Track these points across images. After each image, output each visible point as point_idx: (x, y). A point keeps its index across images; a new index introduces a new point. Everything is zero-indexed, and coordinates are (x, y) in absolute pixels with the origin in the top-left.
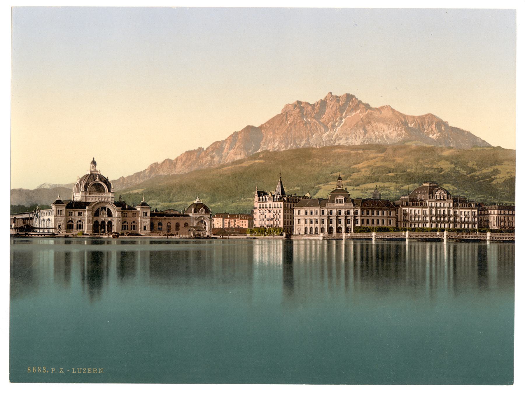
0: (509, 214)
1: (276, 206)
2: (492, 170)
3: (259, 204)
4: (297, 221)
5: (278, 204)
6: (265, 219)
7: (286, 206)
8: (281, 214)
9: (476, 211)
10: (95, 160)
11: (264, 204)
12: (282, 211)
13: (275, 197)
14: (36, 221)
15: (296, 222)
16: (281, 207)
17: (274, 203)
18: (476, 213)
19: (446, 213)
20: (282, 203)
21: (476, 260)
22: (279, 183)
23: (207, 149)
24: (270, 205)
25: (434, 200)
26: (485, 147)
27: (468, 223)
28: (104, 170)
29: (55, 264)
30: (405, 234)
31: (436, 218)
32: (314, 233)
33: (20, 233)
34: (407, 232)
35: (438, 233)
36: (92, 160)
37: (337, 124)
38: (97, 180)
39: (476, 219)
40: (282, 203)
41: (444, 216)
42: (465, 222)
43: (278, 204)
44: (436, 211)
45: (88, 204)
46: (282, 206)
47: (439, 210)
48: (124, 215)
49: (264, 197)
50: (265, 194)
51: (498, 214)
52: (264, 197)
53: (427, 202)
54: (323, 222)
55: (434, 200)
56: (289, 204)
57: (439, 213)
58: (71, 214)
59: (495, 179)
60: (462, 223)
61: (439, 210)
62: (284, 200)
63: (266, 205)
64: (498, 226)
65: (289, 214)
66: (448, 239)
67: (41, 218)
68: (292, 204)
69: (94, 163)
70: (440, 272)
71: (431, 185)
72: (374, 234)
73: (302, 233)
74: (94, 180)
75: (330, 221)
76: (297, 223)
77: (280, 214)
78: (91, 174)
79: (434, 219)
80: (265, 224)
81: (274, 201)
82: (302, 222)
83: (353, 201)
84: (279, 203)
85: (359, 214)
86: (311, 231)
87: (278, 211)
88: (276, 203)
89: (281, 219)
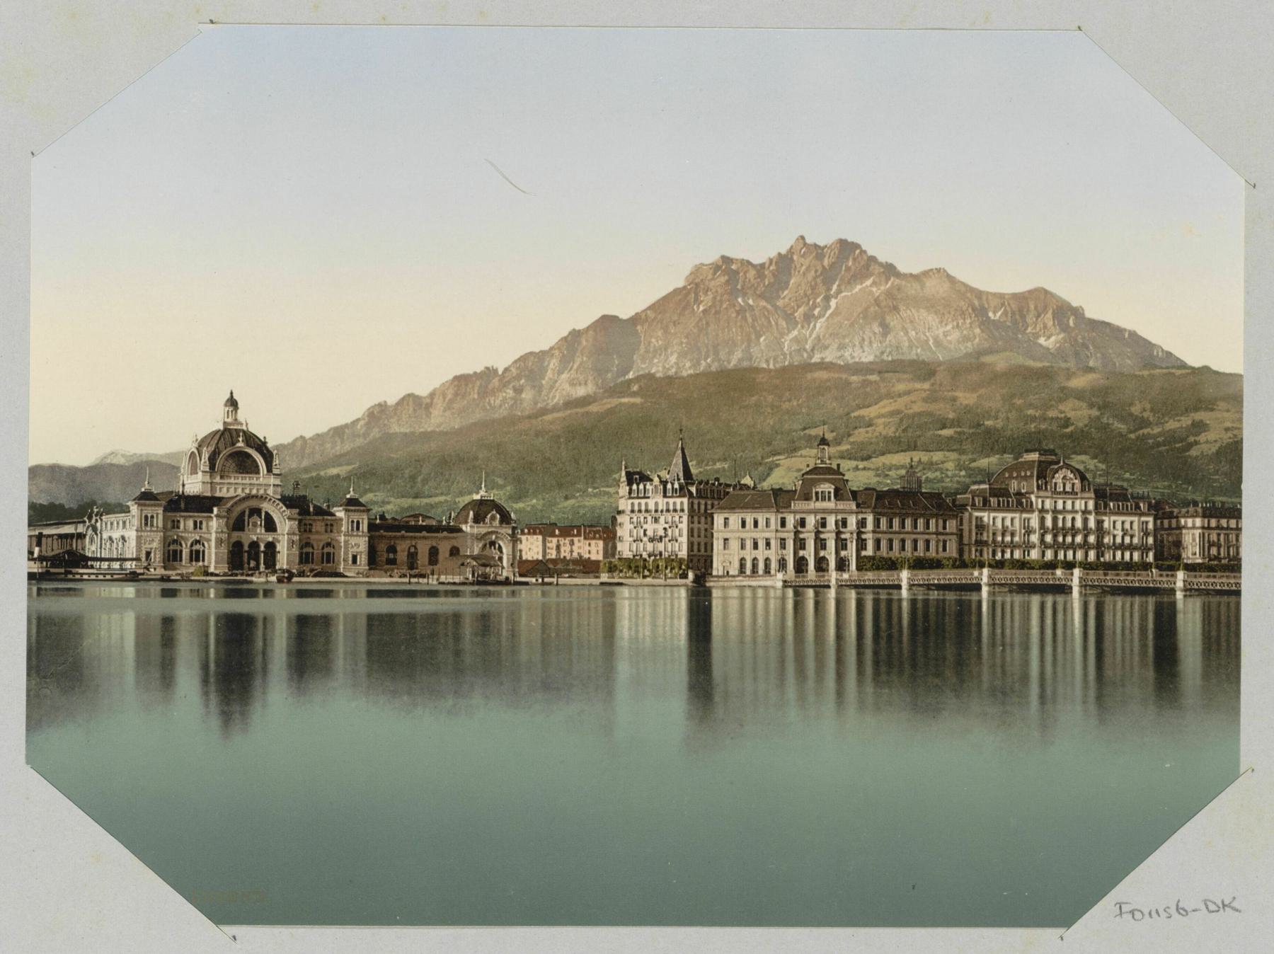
1: (671, 508)
2: (1190, 422)
4: (721, 542)
5: (675, 504)
7: (696, 507)
8: (684, 526)
10: (235, 397)
11: (643, 501)
12: (685, 519)
13: (669, 486)
14: (92, 541)
15: (718, 545)
16: (682, 510)
18: (1151, 526)
19: (1079, 524)
20: (685, 500)
22: (679, 452)
23: (506, 370)
24: (656, 504)
26: (1173, 367)
30: (981, 574)
31: (1055, 536)
32: (761, 572)
33: (52, 570)
34: (1077, 572)
35: (1059, 572)
36: (228, 396)
37: (816, 312)
39: (1151, 540)
40: (685, 500)
42: (1123, 547)
43: (675, 504)
44: (1055, 520)
45: (218, 501)
46: (686, 507)
50: (645, 478)
51: (1203, 528)
52: (641, 486)
53: (1033, 499)
54: (783, 546)
55: (1049, 494)
56: (703, 502)
57: (1060, 525)
58: (175, 525)
59: (1196, 443)
61: (1061, 517)
62: (690, 493)
63: (646, 504)
65: (703, 526)
66: (1083, 586)
67: (105, 536)
71: (1043, 458)
73: (734, 571)
74: (233, 444)
75: (800, 544)
78: (226, 430)
79: (1049, 538)
80: (645, 549)
82: (734, 544)
83: (855, 494)
84: (678, 501)
86: (755, 566)
87: (677, 519)
88: (671, 501)
89: (684, 539)
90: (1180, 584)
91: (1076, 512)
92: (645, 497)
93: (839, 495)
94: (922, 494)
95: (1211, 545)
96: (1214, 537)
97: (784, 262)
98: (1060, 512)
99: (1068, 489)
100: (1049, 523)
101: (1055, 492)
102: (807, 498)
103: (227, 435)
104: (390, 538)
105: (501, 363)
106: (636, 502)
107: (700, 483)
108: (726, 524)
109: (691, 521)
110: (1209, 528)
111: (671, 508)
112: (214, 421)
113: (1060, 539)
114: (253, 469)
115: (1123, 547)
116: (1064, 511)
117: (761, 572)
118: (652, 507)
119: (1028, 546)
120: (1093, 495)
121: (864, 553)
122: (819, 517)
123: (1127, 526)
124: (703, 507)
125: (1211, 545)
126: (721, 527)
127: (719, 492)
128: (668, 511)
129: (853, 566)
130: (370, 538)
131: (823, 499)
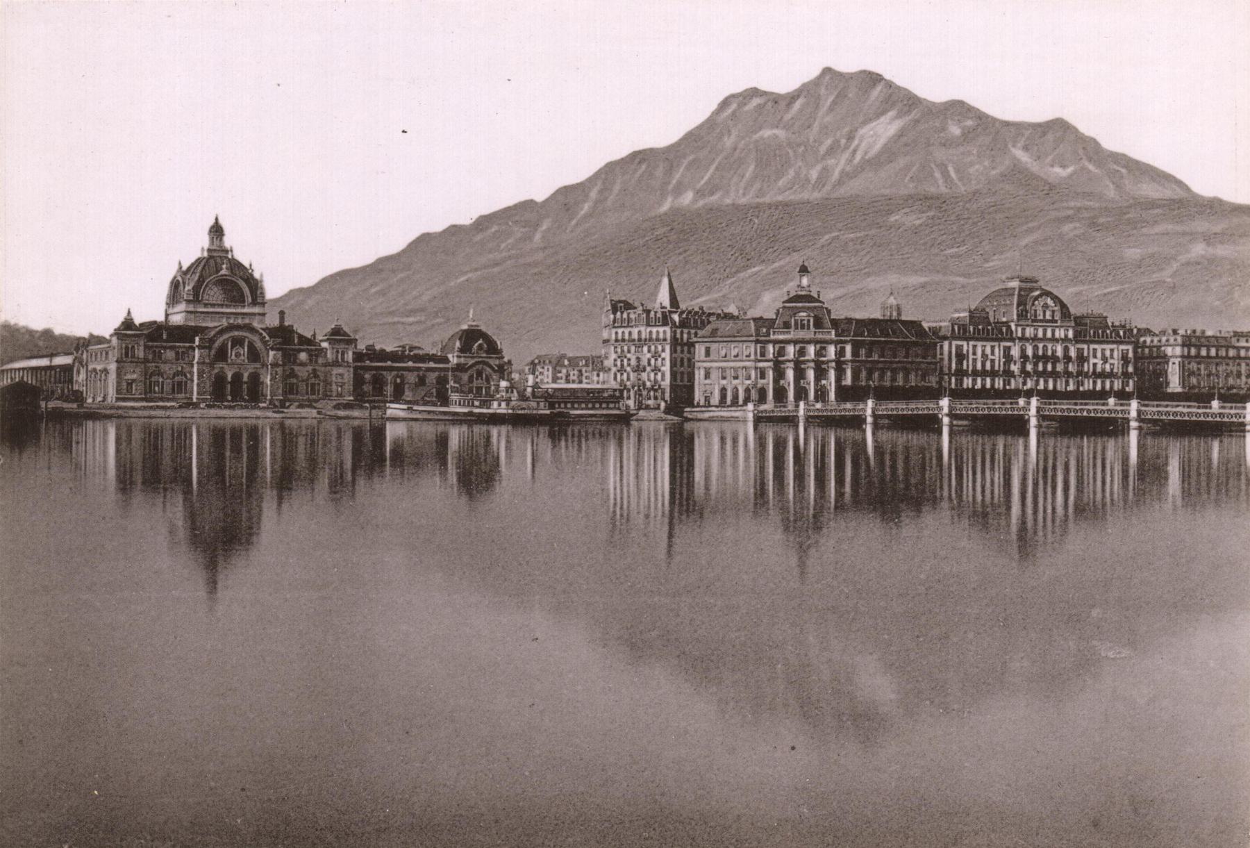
0: (1208, 357)
1: (654, 336)
3: (614, 331)
4: (702, 372)
5: (658, 332)
6: (628, 369)
7: (678, 336)
8: (667, 355)
9: (1130, 348)
10: (221, 221)
11: (627, 331)
12: (668, 348)
13: (652, 314)
14: (78, 372)
15: (699, 375)
16: (665, 340)
17: (649, 329)
18: (1131, 355)
19: (1060, 353)
20: (668, 329)
21: (752, 464)
22: (665, 281)
24: (640, 332)
25: (1030, 322)
27: (1111, 375)
28: (242, 247)
29: (118, 476)
30: (1029, 403)
31: (1036, 365)
32: (729, 402)
34: (1034, 402)
35: (1112, 401)
36: (212, 222)
38: (224, 272)
39: (1131, 369)
40: (668, 329)
41: (1055, 360)
42: (984, 374)
43: (658, 332)
44: (1036, 348)
45: (197, 330)
46: (668, 336)
47: (1041, 346)
48: (289, 358)
49: (625, 316)
50: (628, 306)
51: (1182, 356)
52: (625, 316)
53: (1013, 328)
54: (763, 376)
55: (1030, 322)
56: (686, 331)
57: (1040, 353)
58: (158, 356)
60: (975, 373)
61: (1041, 346)
62: (674, 323)
63: (630, 333)
64: (1184, 387)
65: (686, 356)
66: (1041, 417)
67: (90, 367)
68: (693, 331)
69: (217, 231)
70: (688, 500)
71: (1024, 285)
72: (945, 402)
73: (715, 400)
74: (218, 271)
75: (779, 374)
76: (702, 375)
77: (663, 355)
78: (210, 257)
79: (1029, 367)
80: (628, 379)
81: (648, 325)
82: (715, 375)
83: (835, 323)
84: (661, 329)
85: (848, 355)
86: (735, 397)
87: (660, 348)
88: (654, 330)
89: (667, 368)
90: (1134, 414)
91: (1021, 339)
92: (628, 326)
93: (818, 324)
94: (904, 323)
95: (1192, 373)
96: (1194, 366)
97: (807, 90)
98: (1041, 340)
99: (1048, 317)
100: (1030, 352)
101: (1035, 321)
102: (787, 325)
103: (212, 261)
104: (377, 368)
105: (540, 194)
106: (620, 331)
107: (682, 312)
108: (708, 353)
109: (673, 351)
110: (1189, 356)
111: (654, 336)
112: (195, 247)
113: (1040, 368)
114: (240, 300)
115: (984, 374)
116: (1044, 339)
117: (729, 402)
118: (635, 336)
119: (1008, 374)
120: (1073, 324)
121: (844, 383)
122: (798, 347)
123: (1108, 353)
124: (685, 336)
125: (1192, 373)
126: (703, 357)
127: (702, 322)
128: (651, 339)
129: (832, 396)
130: (356, 368)
131: (803, 327)
